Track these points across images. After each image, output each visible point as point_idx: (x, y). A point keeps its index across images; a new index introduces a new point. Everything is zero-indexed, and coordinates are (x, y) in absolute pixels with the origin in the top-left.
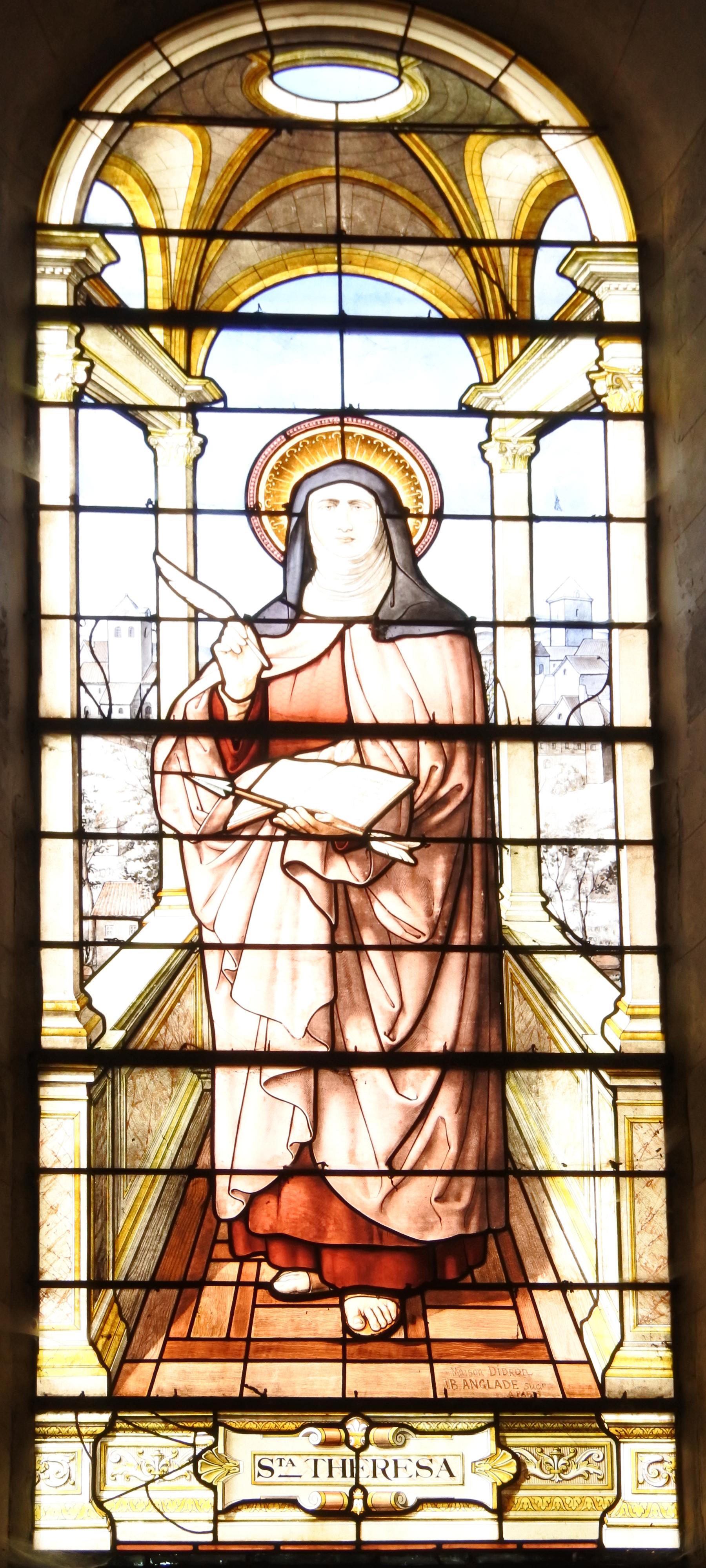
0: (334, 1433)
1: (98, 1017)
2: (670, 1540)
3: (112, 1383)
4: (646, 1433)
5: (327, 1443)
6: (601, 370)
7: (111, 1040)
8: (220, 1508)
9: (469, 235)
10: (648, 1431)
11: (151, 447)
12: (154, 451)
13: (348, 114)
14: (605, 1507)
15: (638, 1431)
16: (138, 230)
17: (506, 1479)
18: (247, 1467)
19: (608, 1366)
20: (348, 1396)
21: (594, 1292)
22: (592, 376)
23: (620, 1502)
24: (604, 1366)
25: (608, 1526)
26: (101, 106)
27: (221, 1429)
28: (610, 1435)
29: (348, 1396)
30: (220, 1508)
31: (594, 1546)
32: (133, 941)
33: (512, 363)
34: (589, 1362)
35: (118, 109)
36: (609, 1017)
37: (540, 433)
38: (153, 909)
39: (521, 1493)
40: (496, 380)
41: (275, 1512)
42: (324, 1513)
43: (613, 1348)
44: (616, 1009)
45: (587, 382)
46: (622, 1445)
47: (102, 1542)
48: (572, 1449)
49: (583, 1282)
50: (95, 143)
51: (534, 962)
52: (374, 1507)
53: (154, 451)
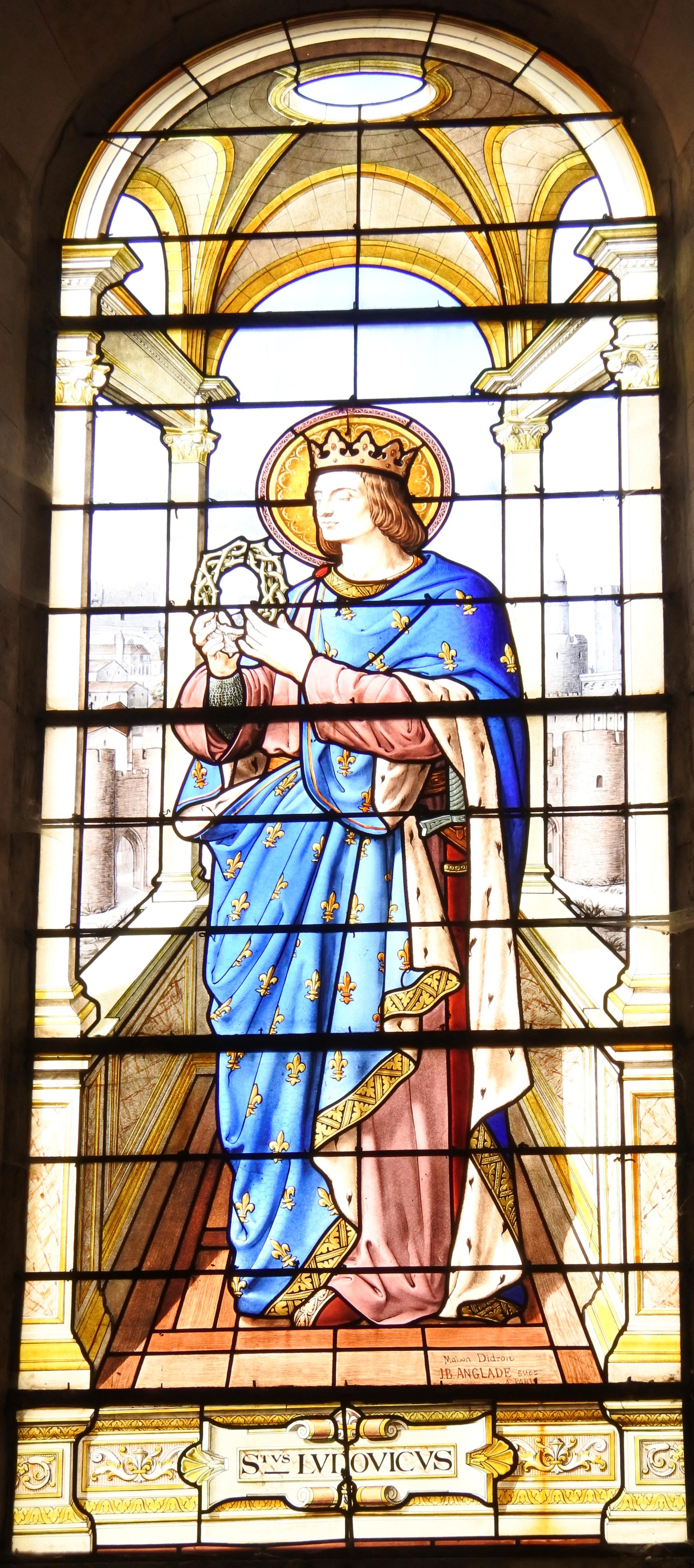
0: (327, 1425)
1: (92, 1005)
2: (678, 1534)
3: (97, 1375)
4: (650, 1420)
5: (319, 1438)
6: (616, 348)
7: (105, 1028)
8: (205, 1507)
9: (488, 222)
10: (653, 1417)
11: (166, 445)
12: (169, 449)
13: (369, 115)
14: (608, 1500)
15: (643, 1417)
16: (163, 238)
17: (503, 1471)
18: (233, 1464)
19: (611, 1352)
20: (337, 1384)
21: (597, 1274)
22: (605, 355)
23: (623, 1493)
24: (606, 1352)
25: (611, 1520)
26: (129, 127)
27: (206, 1424)
28: (612, 1422)
29: (337, 1384)
30: (205, 1507)
31: (597, 1541)
32: (130, 926)
33: (526, 346)
34: (591, 1347)
35: (147, 127)
36: (611, 990)
37: (552, 415)
38: (151, 894)
39: (518, 1485)
40: (509, 365)
41: (259, 1511)
42: (317, 1509)
43: (617, 1332)
44: (619, 983)
45: (602, 361)
46: (625, 1433)
47: (81, 1545)
48: (573, 1439)
49: (585, 1262)
50: (125, 156)
51: (536, 937)
52: (362, 1503)
53: (169, 449)
